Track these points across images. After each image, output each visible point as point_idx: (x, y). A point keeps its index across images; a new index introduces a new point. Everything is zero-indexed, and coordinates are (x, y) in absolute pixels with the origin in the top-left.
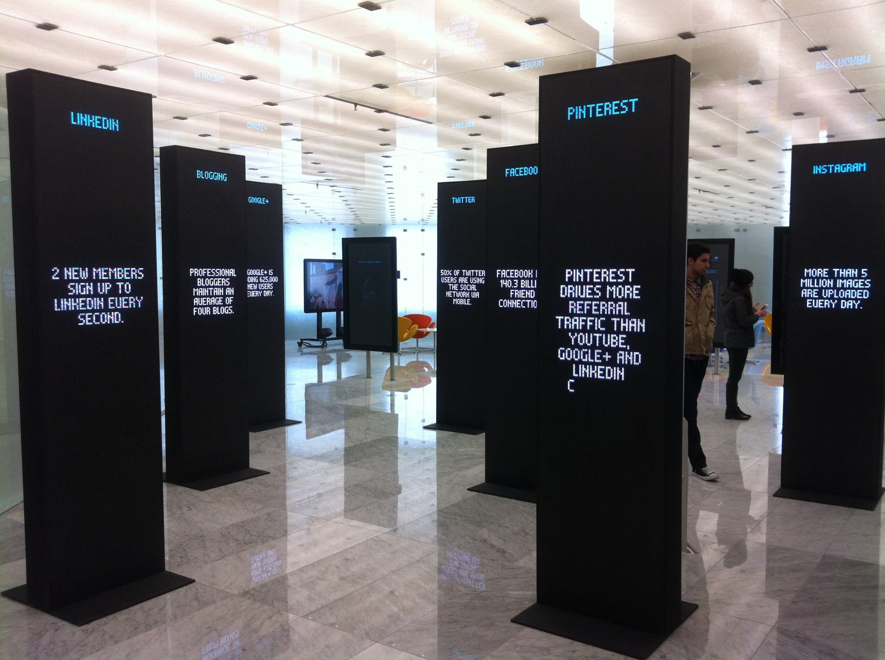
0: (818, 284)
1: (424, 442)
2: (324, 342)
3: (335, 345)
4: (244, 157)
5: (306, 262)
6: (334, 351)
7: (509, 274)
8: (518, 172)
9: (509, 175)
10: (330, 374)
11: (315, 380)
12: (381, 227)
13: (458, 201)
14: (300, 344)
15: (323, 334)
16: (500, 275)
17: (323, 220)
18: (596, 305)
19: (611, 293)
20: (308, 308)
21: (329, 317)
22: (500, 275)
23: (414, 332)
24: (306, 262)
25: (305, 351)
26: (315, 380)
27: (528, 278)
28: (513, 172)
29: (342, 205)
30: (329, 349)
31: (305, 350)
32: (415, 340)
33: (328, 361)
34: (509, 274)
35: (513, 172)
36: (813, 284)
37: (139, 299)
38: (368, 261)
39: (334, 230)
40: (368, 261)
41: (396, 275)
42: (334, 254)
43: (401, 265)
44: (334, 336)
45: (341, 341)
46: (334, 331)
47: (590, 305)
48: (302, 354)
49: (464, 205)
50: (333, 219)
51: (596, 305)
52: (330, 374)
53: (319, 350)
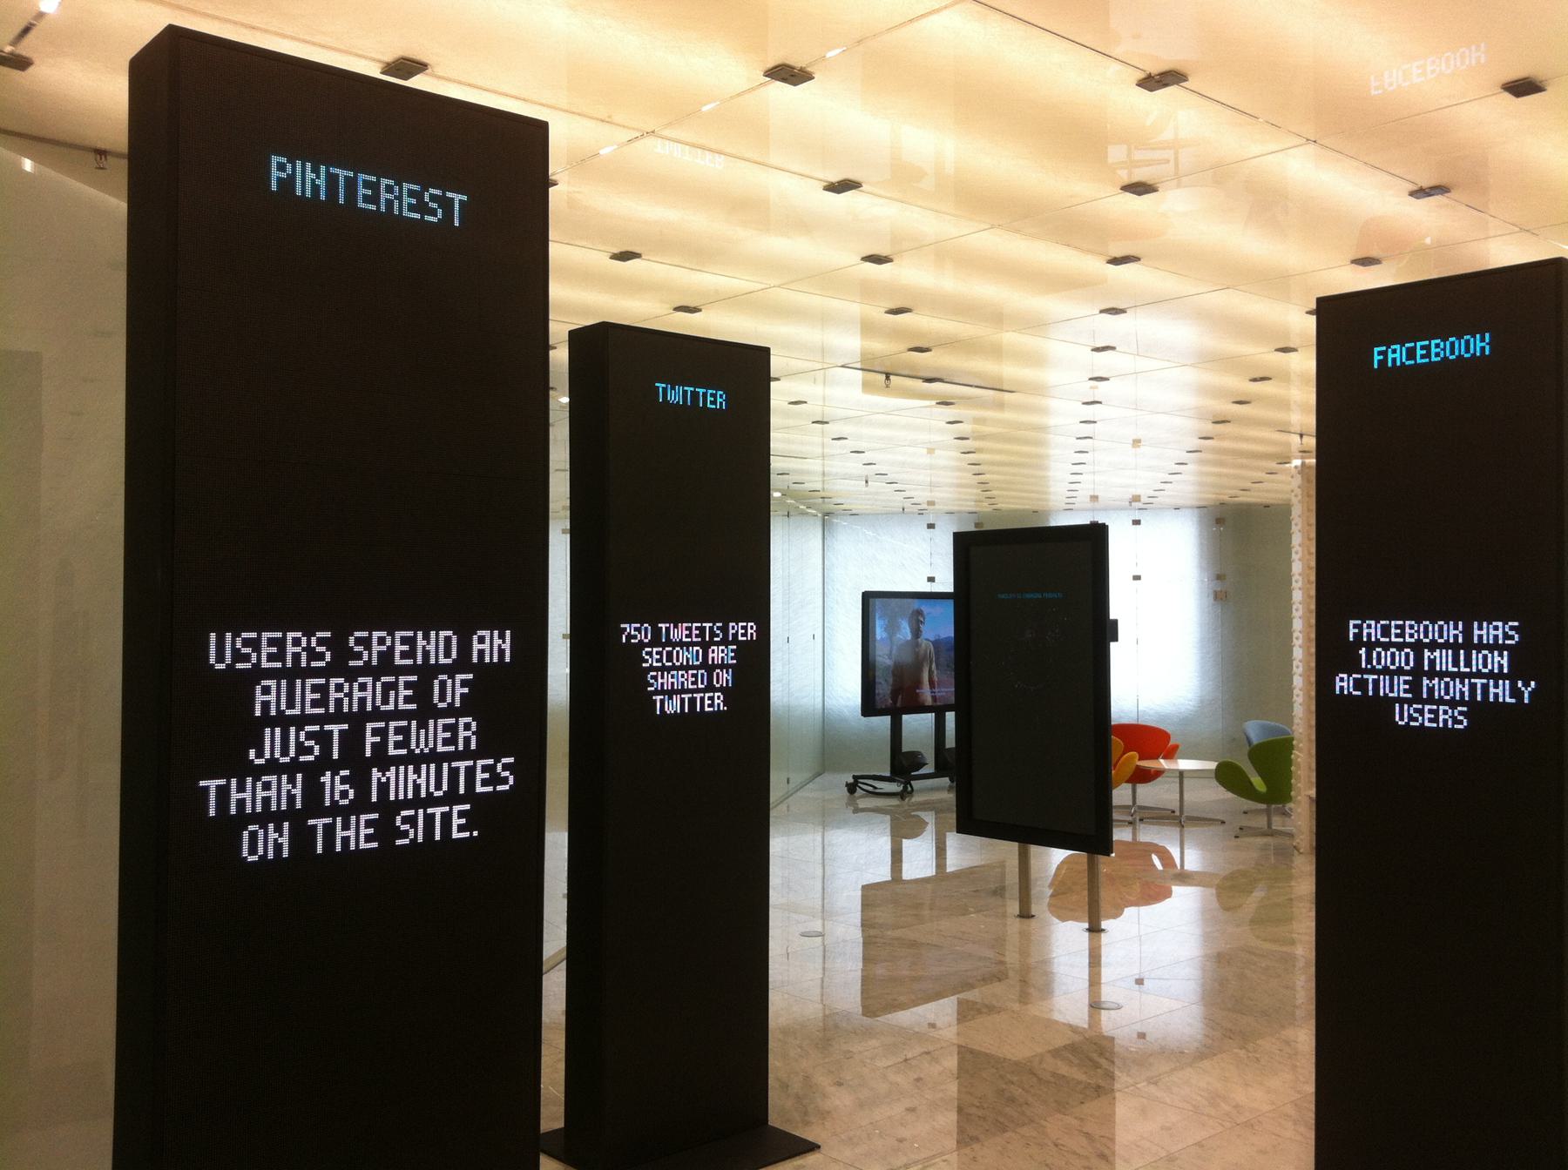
0: (1468, 664)
1: (1142, 1036)
2: (907, 783)
3: (933, 789)
4: (764, 353)
5: (868, 598)
6: (925, 806)
7: (1386, 631)
8: (1411, 354)
9: (1383, 363)
10: (919, 859)
11: (883, 873)
12: (1046, 514)
13: (675, 395)
14: (851, 788)
15: (903, 766)
16: (1358, 636)
17: (907, 504)
18: (398, 731)
19: (1431, 690)
20: (869, 706)
21: (918, 726)
22: (1358, 636)
23: (1129, 771)
24: (868, 598)
25: (862, 803)
26: (883, 873)
27: (1446, 645)
28: (1397, 354)
29: (949, 457)
30: (916, 799)
31: (863, 803)
32: (1129, 786)
33: (915, 830)
34: (1386, 631)
35: (1397, 354)
36: (1456, 663)
37: (1527, 685)
38: (1027, 594)
39: (931, 526)
40: (1027, 594)
41: (1106, 631)
42: (931, 579)
43: (1119, 606)
44: (929, 769)
45: (946, 781)
46: (929, 756)
47: (383, 732)
48: (857, 810)
49: (691, 410)
50: (931, 503)
51: (398, 731)
52: (919, 859)
53: (895, 802)
